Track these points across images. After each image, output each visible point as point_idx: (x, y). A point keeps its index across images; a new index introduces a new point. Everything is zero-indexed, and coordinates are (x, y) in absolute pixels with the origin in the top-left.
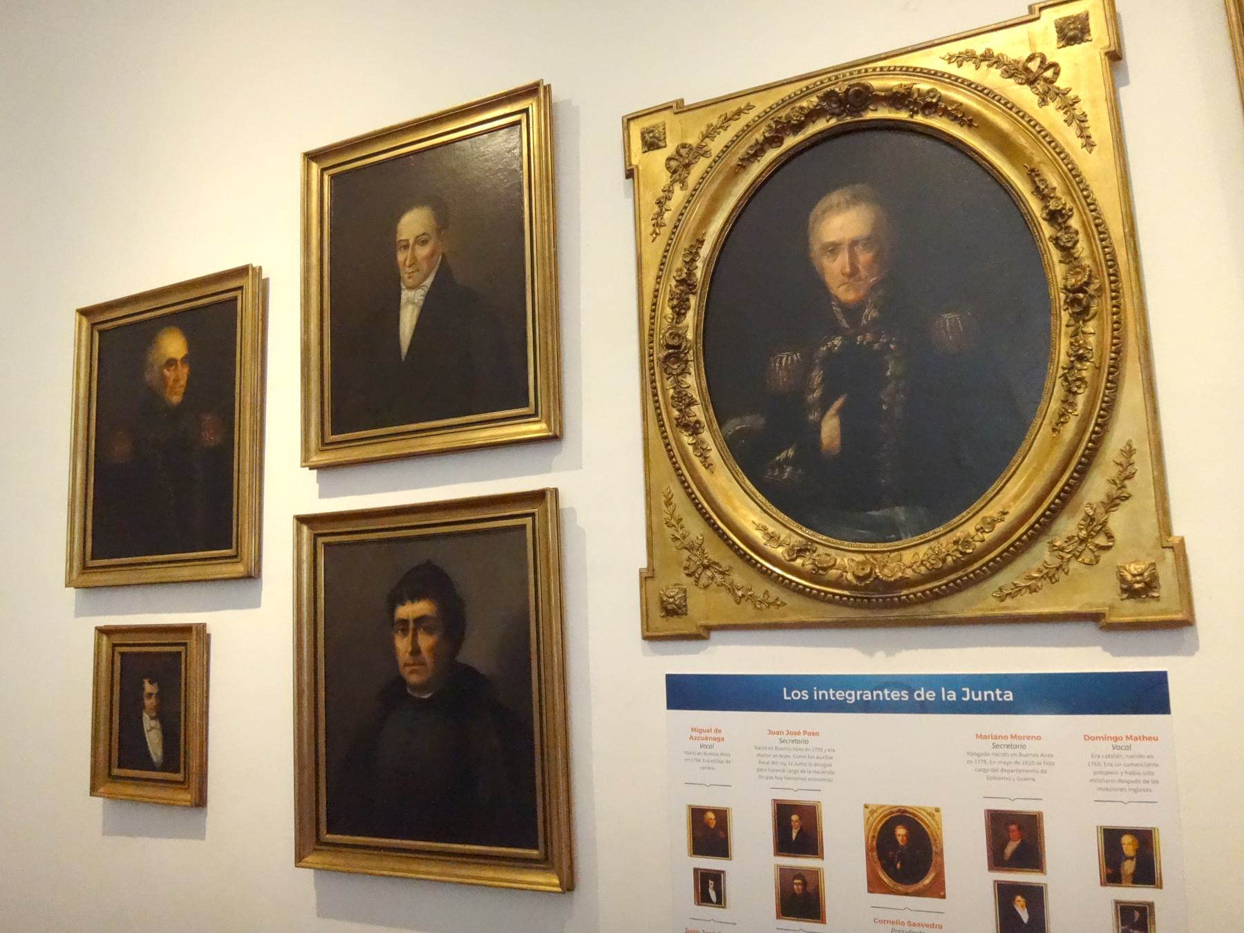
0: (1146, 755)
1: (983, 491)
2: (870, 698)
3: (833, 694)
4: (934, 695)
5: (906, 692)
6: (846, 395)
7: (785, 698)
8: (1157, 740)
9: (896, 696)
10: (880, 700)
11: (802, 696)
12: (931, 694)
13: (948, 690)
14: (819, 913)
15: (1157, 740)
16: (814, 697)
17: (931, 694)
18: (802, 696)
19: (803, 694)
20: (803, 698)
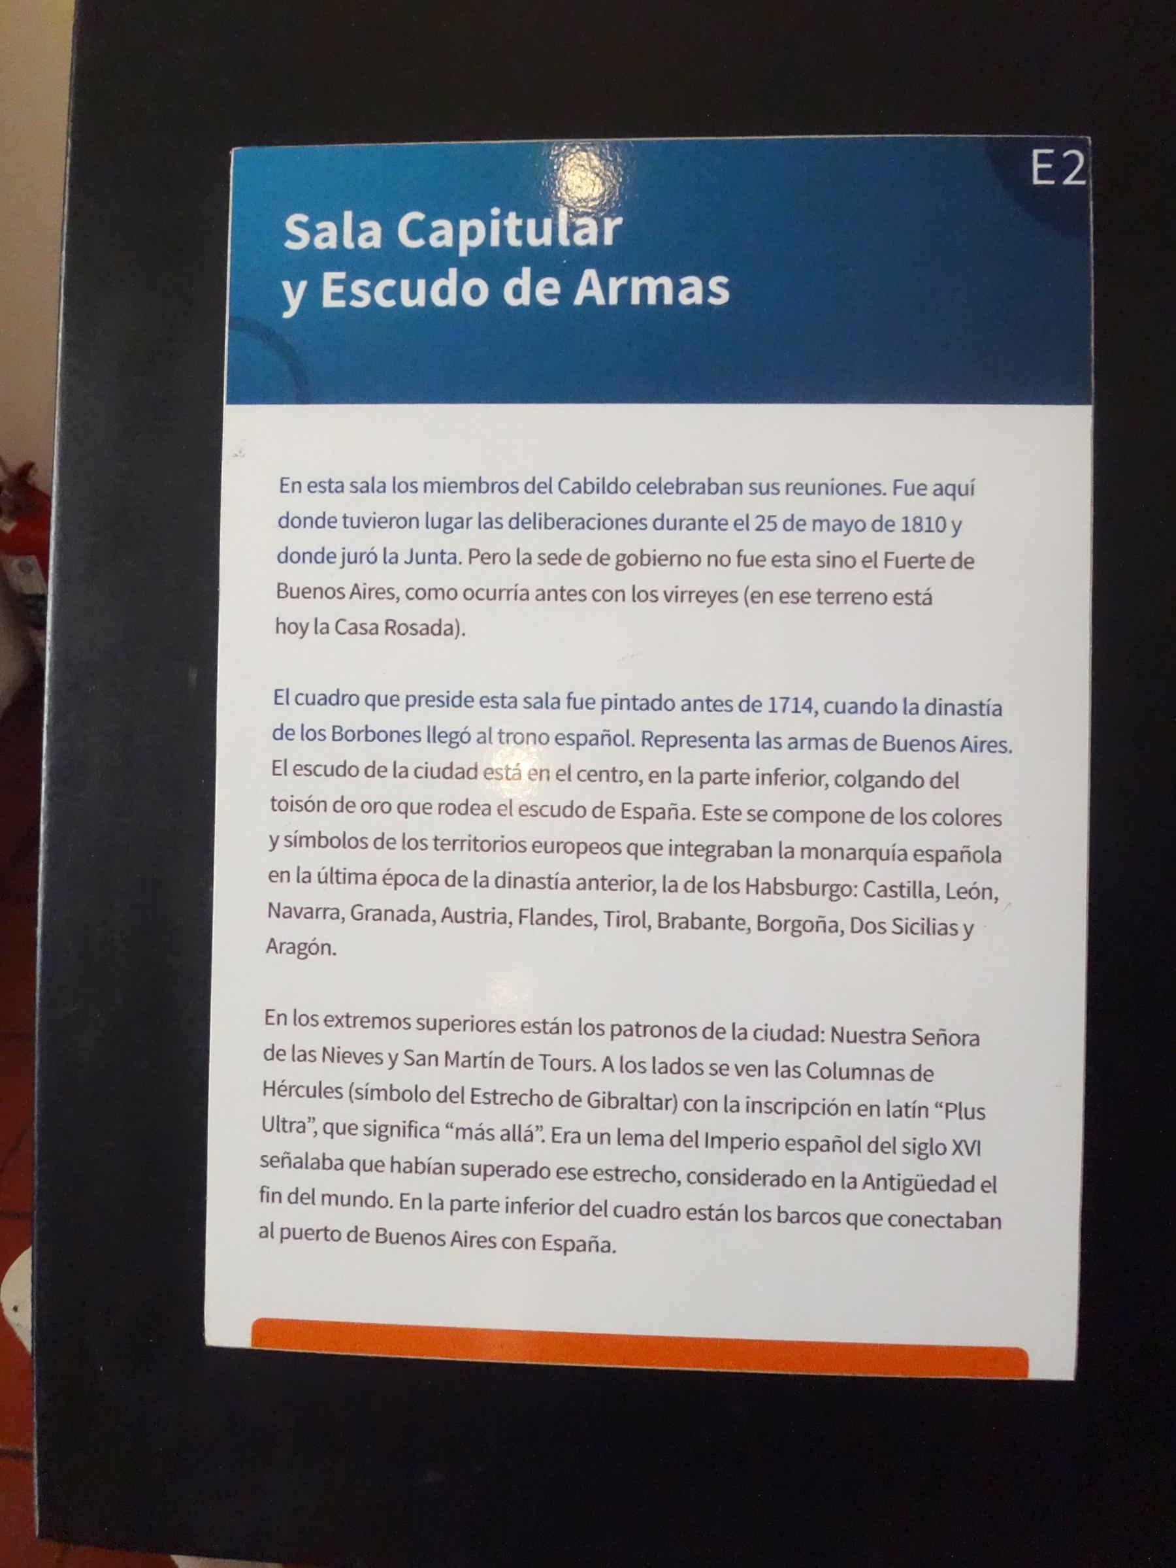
0: (789, 604)
1: (71, 187)
2: (332, 244)
3: (518, 228)
4: (557, 289)
5: (724, 280)
6: (30, 1250)
7: (1036, 153)
8: (929, 601)
9: (549, 291)
10: (285, 240)
11: (371, 290)
12: (549, 286)
13: (362, 220)
14: (73, 132)
15: (929, 601)
16: (1049, 185)
17: (549, 286)
18: (371, 290)
19: (304, 235)
20: (366, 283)
